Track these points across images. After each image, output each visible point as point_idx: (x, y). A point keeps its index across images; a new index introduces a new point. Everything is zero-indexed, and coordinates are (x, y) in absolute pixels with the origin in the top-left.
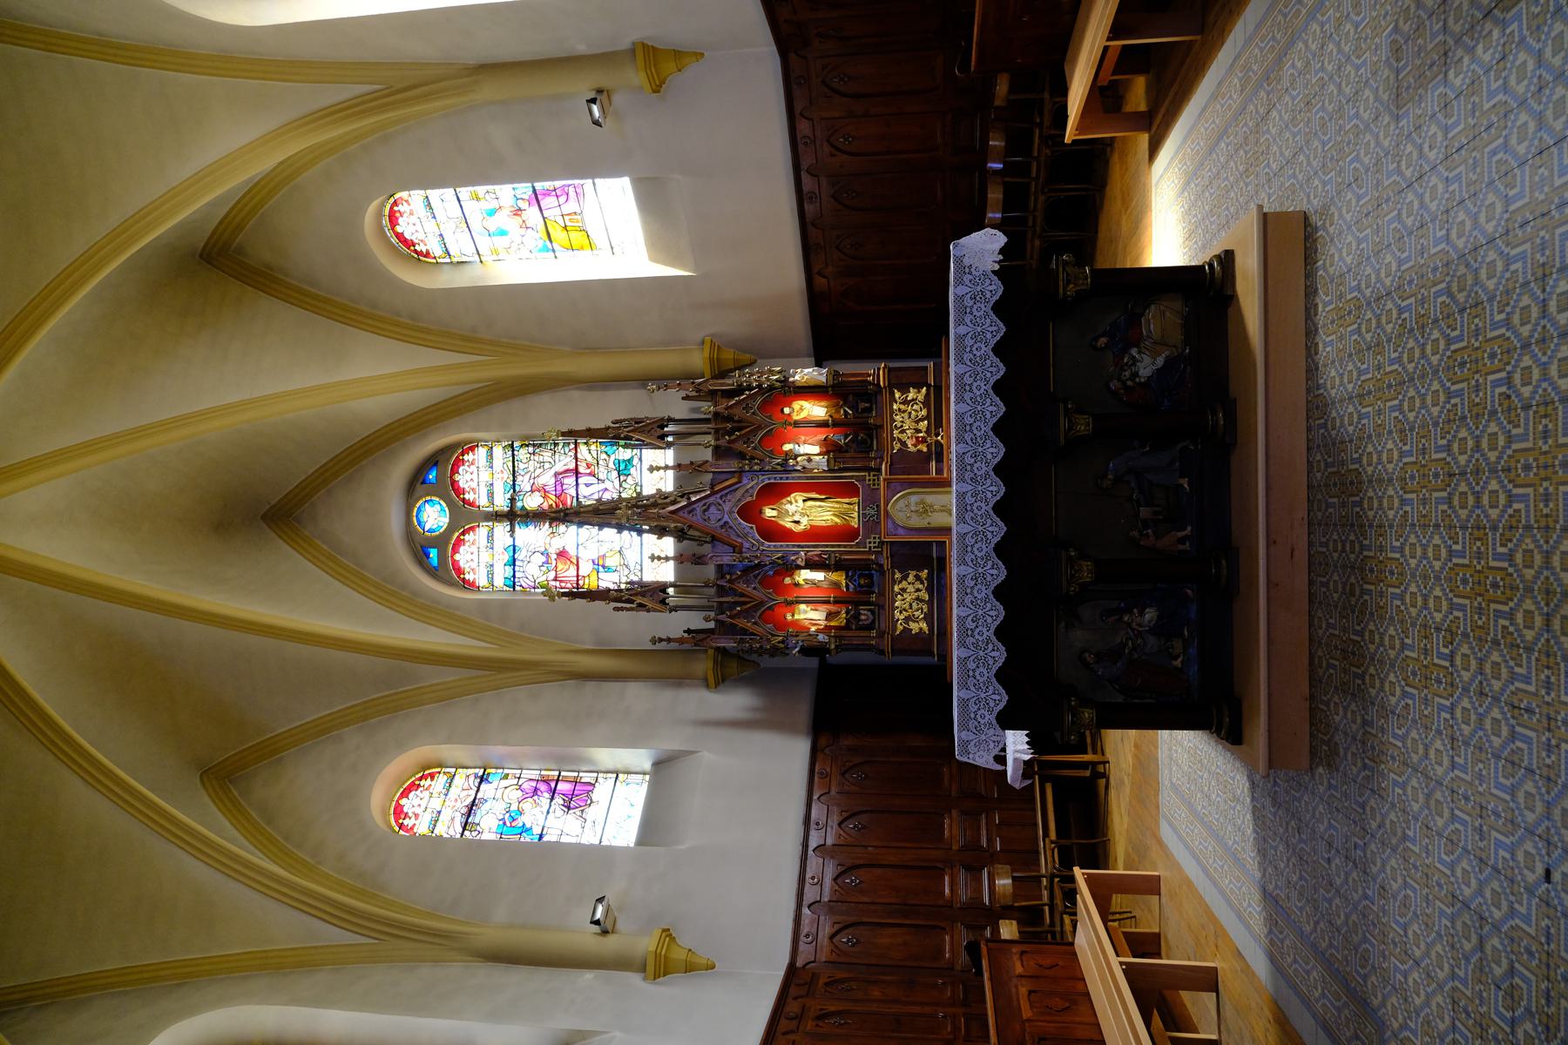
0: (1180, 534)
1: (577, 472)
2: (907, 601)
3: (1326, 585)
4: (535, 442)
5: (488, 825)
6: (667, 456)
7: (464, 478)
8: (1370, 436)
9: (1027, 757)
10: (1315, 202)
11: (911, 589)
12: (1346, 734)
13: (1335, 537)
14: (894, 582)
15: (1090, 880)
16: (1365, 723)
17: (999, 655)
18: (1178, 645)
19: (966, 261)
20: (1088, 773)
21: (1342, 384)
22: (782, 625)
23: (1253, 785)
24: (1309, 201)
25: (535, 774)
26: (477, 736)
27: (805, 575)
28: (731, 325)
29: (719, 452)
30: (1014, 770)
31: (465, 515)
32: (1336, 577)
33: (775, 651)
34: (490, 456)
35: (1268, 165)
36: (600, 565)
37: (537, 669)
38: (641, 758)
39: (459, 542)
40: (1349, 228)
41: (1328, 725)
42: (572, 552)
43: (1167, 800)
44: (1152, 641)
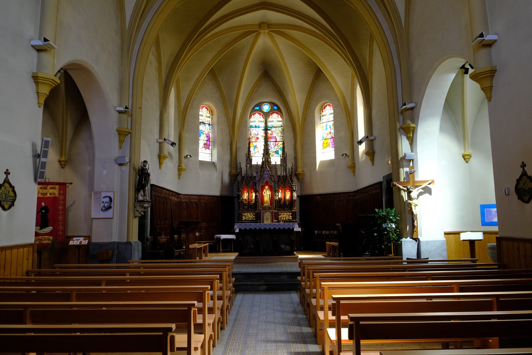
1: (276, 142)
2: (249, 216)
4: (283, 132)
5: (201, 127)
6: (279, 163)
7: (275, 115)
15: (206, 246)
17: (248, 229)
22: (244, 190)
25: (211, 136)
26: (219, 124)
27: (254, 195)
28: (307, 178)
29: (279, 176)
31: (266, 115)
33: (238, 189)
34: (280, 121)
36: (256, 147)
37: (233, 136)
38: (215, 160)
39: (260, 114)
42: (258, 141)
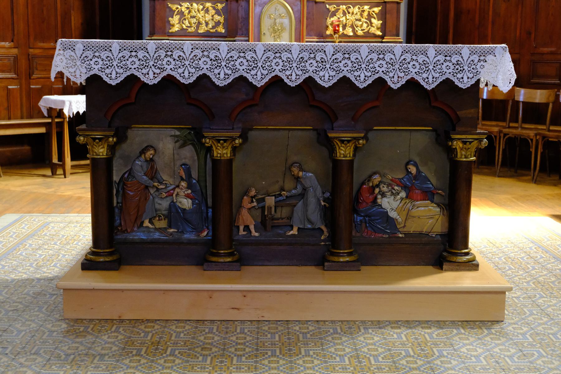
0: (252, 228)
3: (211, 332)
8: (326, 362)
9: (66, 112)
10: (510, 328)
11: (208, 17)
12: (94, 343)
13: (248, 338)
14: (214, 3)
16: (102, 356)
18: (163, 224)
19: (490, 58)
20: (55, 160)
21: (367, 344)
23: (51, 280)
24: (510, 324)
30: (55, 101)
32: (216, 338)
35: (542, 297)
40: (488, 350)
41: (100, 331)
43: (36, 220)
44: (164, 204)
